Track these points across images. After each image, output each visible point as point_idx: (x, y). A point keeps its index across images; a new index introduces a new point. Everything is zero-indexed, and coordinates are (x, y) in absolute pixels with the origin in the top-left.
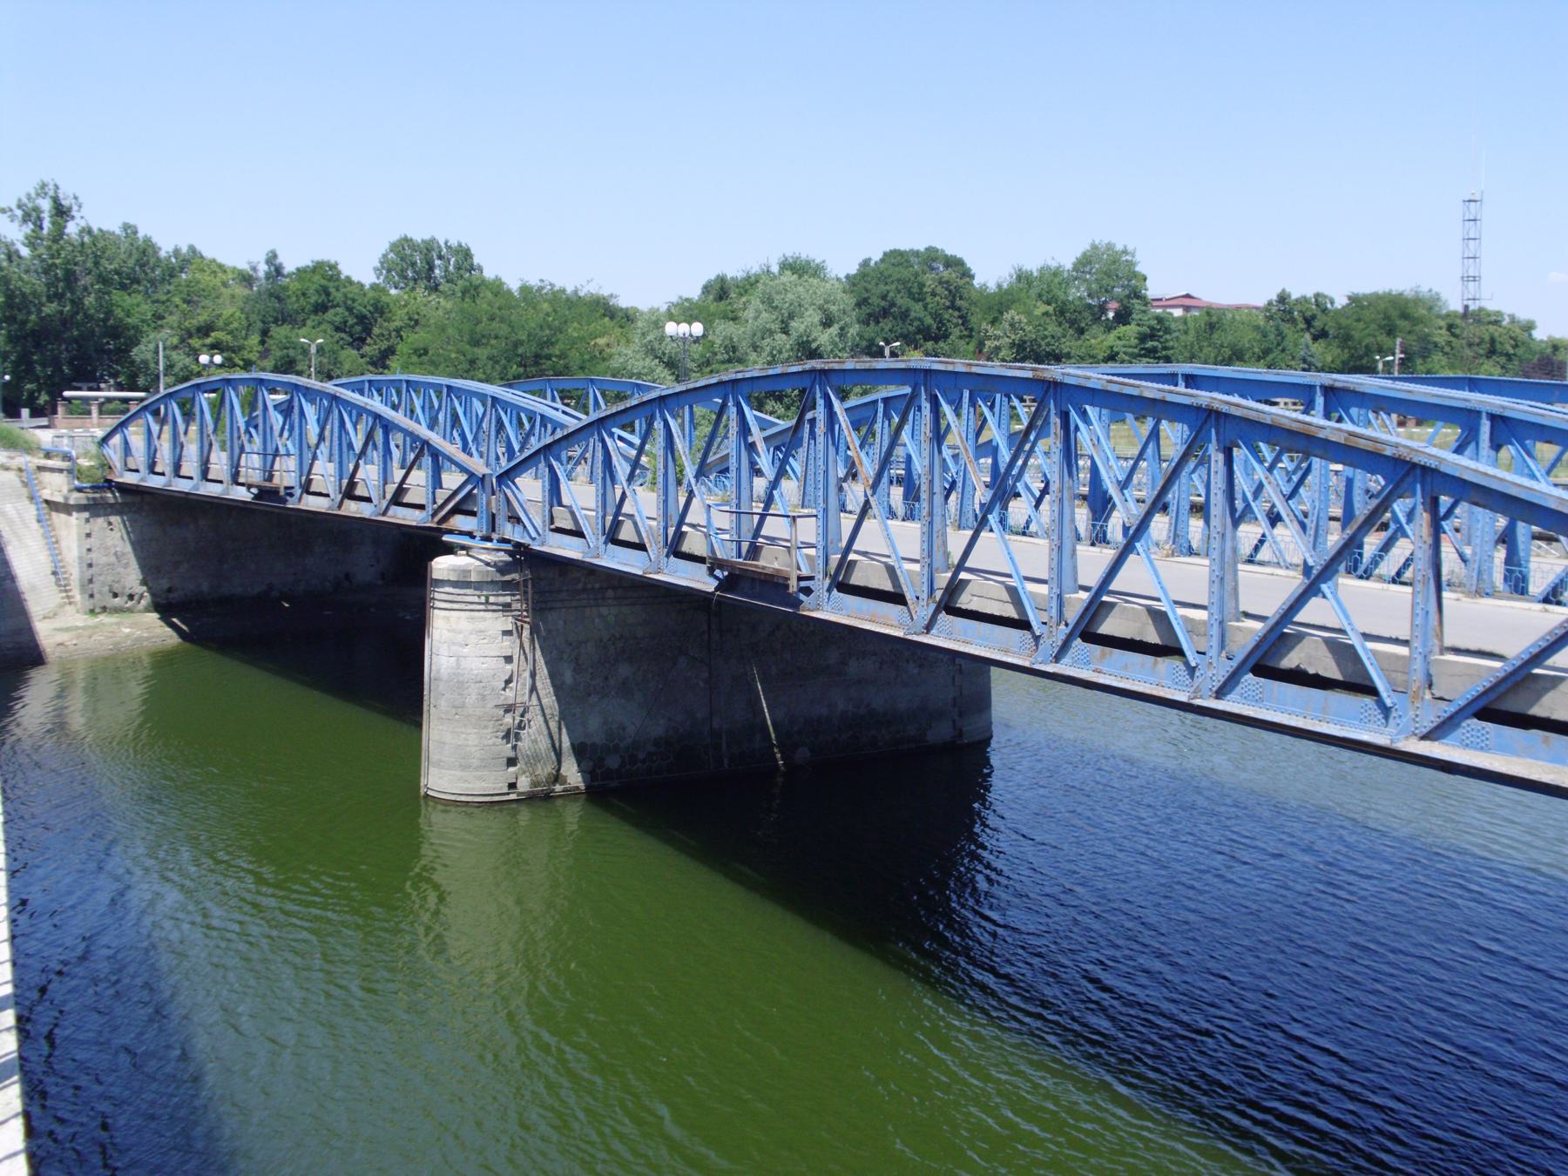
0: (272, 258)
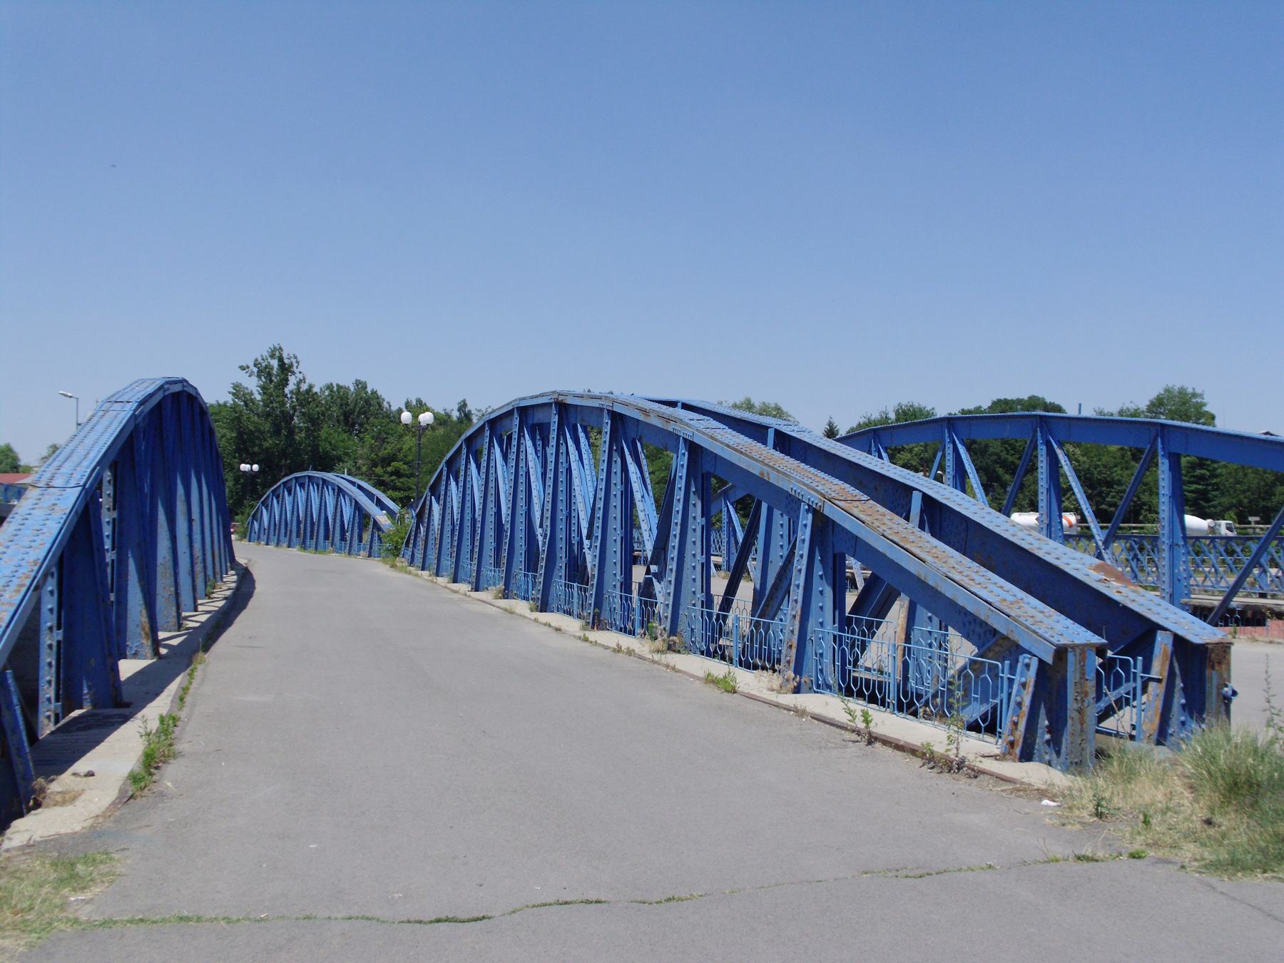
0: (462, 406)
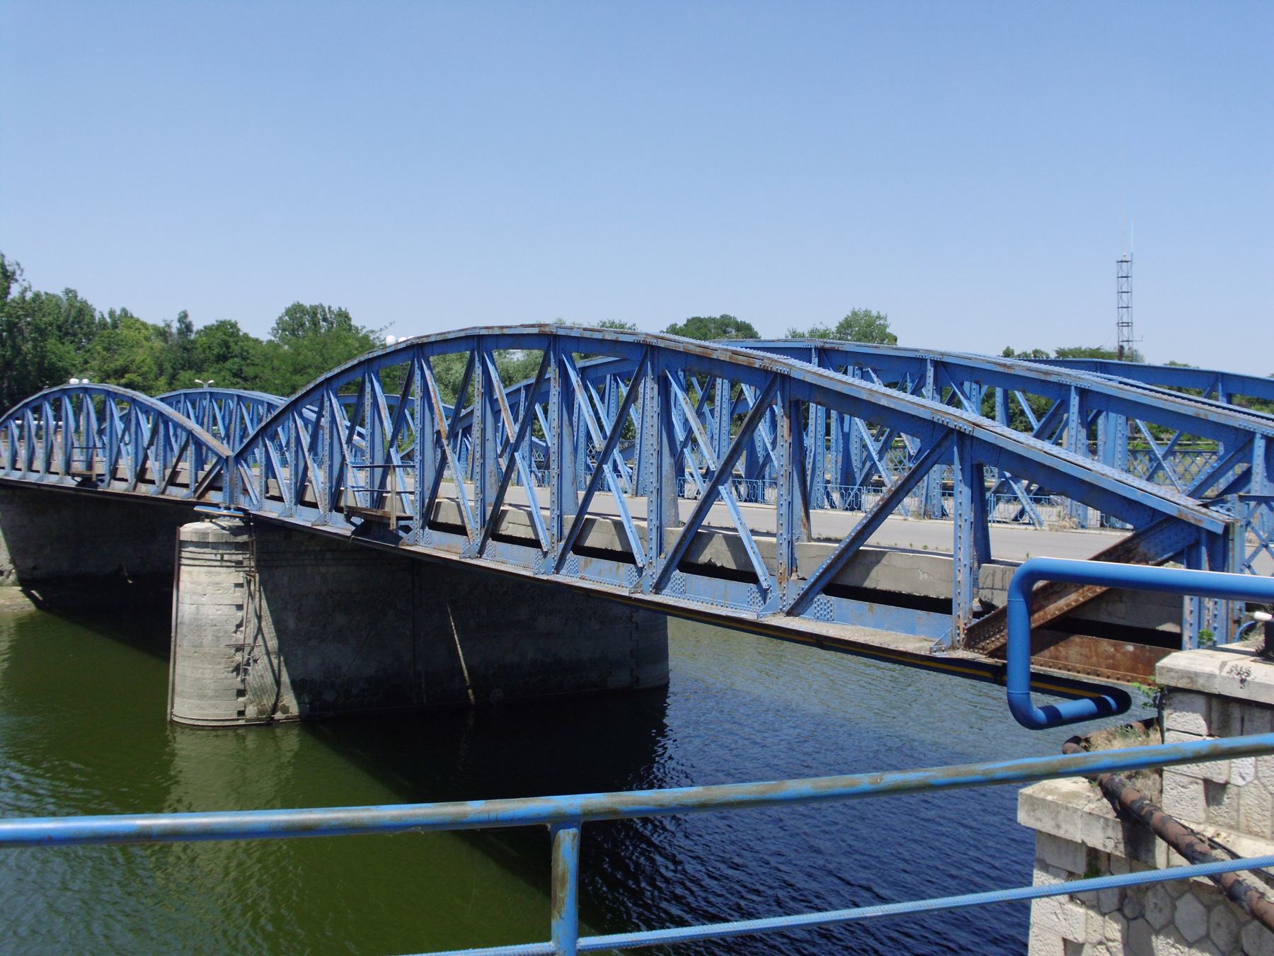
0: (183, 318)
